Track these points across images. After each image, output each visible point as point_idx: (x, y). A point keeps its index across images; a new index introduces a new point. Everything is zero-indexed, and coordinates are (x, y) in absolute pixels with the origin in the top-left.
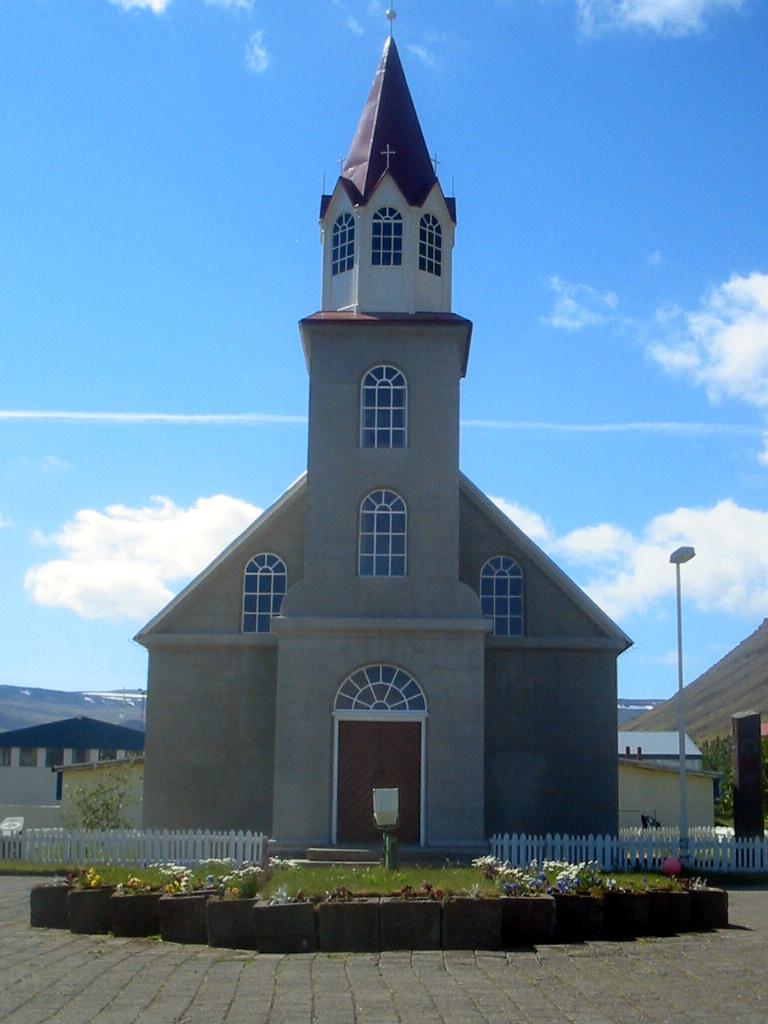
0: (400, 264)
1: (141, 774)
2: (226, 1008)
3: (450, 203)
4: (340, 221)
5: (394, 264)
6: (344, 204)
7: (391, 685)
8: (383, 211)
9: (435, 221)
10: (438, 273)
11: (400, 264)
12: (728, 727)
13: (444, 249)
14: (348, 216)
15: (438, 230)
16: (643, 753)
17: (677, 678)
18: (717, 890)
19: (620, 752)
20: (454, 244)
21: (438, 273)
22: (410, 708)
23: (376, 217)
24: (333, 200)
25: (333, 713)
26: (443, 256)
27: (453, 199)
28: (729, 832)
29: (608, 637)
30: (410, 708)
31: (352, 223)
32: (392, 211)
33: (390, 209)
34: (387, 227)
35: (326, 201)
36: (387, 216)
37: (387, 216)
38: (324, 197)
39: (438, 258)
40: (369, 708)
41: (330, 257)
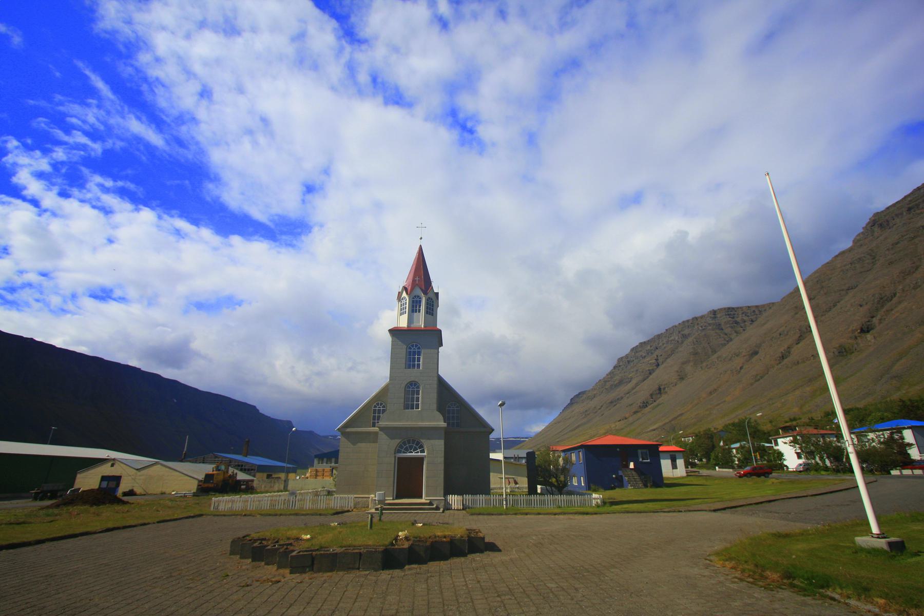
1: (736, 421)
2: (324, 604)
3: (437, 294)
7: (414, 445)
8: (415, 296)
9: (432, 299)
10: (432, 315)
13: (434, 308)
15: (433, 302)
16: (519, 456)
19: (899, 474)
20: (438, 306)
21: (432, 315)
23: (413, 298)
26: (434, 310)
27: (438, 293)
28: (600, 497)
32: (418, 296)
34: (417, 301)
36: (414, 348)
37: (414, 348)
39: (433, 306)
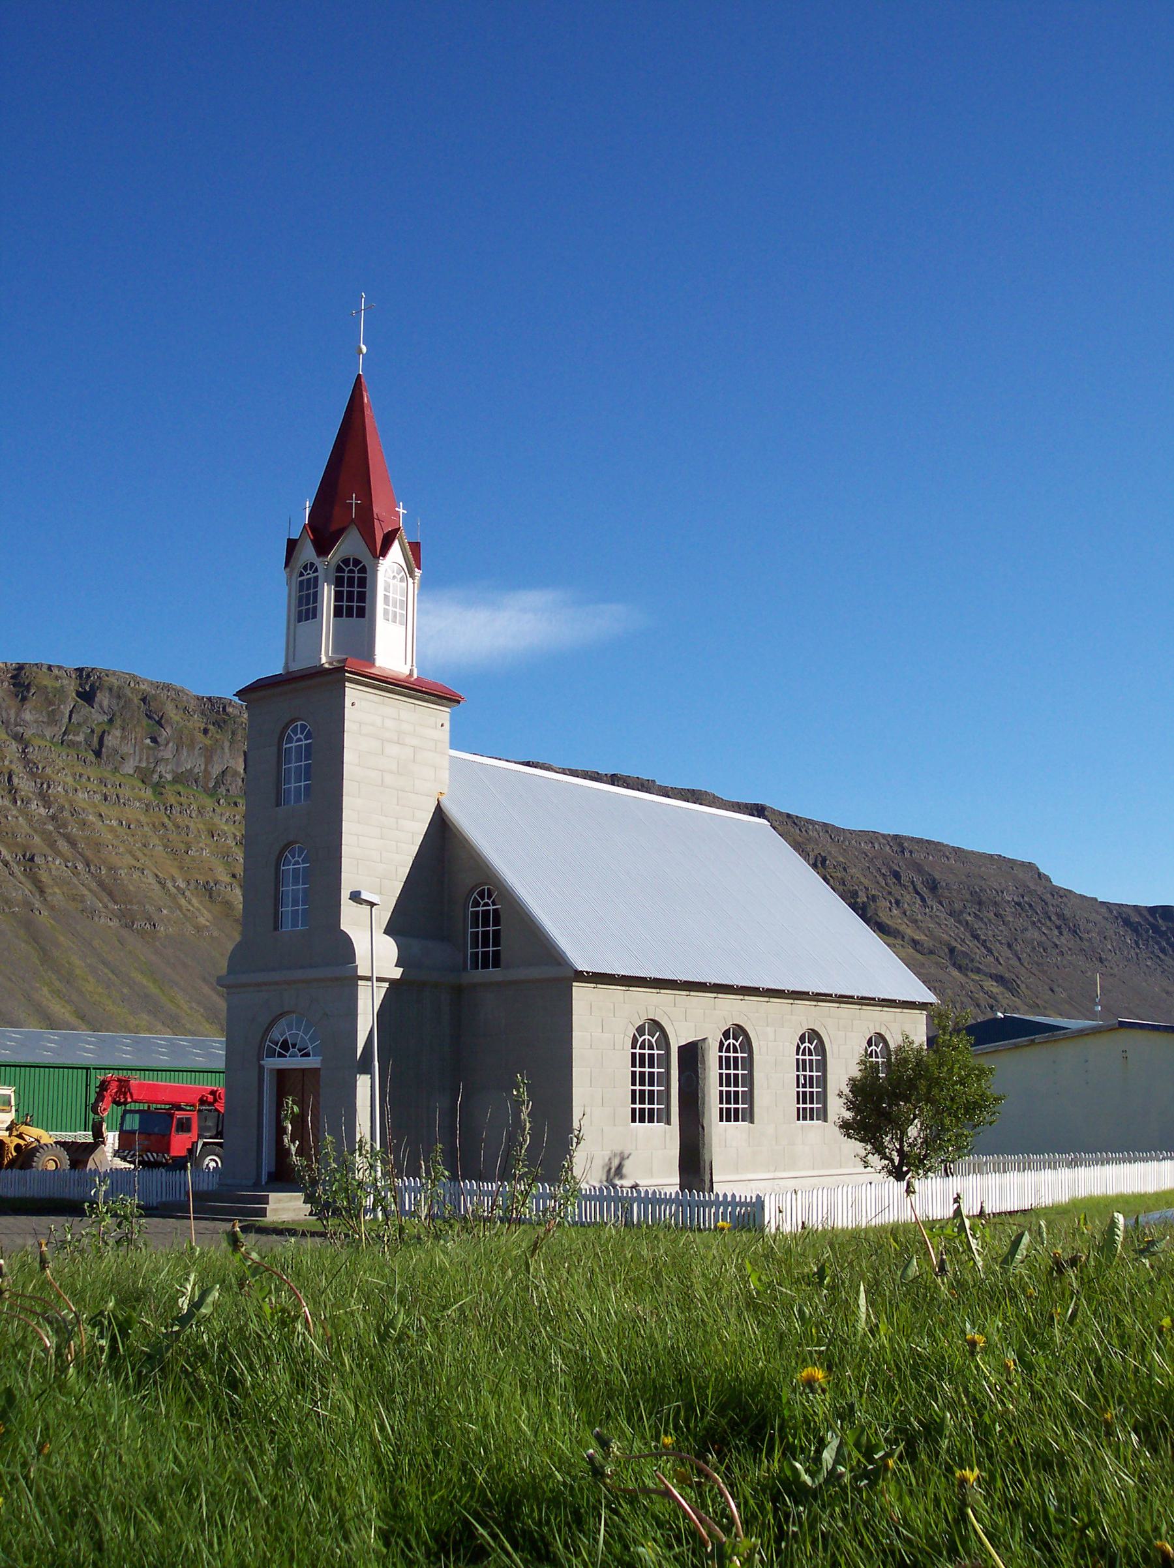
0: (363, 616)
4: (305, 568)
5: (357, 617)
6: (308, 552)
11: (363, 616)
12: (974, 1018)
14: (312, 564)
17: (369, 1104)
18: (862, 1295)
22: (337, 577)
24: (299, 542)
25: (262, 1062)
29: (559, 964)
30: (337, 577)
31: (316, 571)
33: (364, 566)
35: (292, 545)
38: (289, 540)
40: (285, 1056)
41: (294, 602)
